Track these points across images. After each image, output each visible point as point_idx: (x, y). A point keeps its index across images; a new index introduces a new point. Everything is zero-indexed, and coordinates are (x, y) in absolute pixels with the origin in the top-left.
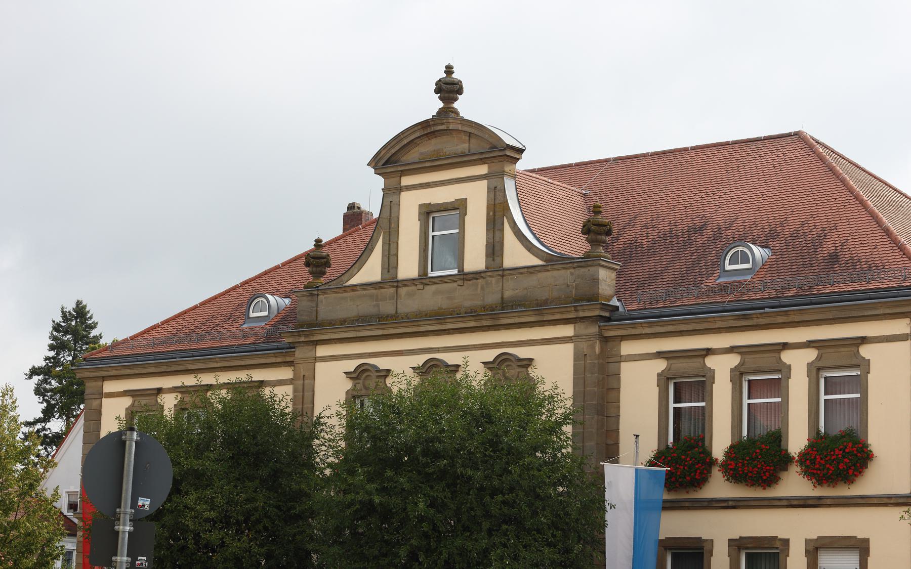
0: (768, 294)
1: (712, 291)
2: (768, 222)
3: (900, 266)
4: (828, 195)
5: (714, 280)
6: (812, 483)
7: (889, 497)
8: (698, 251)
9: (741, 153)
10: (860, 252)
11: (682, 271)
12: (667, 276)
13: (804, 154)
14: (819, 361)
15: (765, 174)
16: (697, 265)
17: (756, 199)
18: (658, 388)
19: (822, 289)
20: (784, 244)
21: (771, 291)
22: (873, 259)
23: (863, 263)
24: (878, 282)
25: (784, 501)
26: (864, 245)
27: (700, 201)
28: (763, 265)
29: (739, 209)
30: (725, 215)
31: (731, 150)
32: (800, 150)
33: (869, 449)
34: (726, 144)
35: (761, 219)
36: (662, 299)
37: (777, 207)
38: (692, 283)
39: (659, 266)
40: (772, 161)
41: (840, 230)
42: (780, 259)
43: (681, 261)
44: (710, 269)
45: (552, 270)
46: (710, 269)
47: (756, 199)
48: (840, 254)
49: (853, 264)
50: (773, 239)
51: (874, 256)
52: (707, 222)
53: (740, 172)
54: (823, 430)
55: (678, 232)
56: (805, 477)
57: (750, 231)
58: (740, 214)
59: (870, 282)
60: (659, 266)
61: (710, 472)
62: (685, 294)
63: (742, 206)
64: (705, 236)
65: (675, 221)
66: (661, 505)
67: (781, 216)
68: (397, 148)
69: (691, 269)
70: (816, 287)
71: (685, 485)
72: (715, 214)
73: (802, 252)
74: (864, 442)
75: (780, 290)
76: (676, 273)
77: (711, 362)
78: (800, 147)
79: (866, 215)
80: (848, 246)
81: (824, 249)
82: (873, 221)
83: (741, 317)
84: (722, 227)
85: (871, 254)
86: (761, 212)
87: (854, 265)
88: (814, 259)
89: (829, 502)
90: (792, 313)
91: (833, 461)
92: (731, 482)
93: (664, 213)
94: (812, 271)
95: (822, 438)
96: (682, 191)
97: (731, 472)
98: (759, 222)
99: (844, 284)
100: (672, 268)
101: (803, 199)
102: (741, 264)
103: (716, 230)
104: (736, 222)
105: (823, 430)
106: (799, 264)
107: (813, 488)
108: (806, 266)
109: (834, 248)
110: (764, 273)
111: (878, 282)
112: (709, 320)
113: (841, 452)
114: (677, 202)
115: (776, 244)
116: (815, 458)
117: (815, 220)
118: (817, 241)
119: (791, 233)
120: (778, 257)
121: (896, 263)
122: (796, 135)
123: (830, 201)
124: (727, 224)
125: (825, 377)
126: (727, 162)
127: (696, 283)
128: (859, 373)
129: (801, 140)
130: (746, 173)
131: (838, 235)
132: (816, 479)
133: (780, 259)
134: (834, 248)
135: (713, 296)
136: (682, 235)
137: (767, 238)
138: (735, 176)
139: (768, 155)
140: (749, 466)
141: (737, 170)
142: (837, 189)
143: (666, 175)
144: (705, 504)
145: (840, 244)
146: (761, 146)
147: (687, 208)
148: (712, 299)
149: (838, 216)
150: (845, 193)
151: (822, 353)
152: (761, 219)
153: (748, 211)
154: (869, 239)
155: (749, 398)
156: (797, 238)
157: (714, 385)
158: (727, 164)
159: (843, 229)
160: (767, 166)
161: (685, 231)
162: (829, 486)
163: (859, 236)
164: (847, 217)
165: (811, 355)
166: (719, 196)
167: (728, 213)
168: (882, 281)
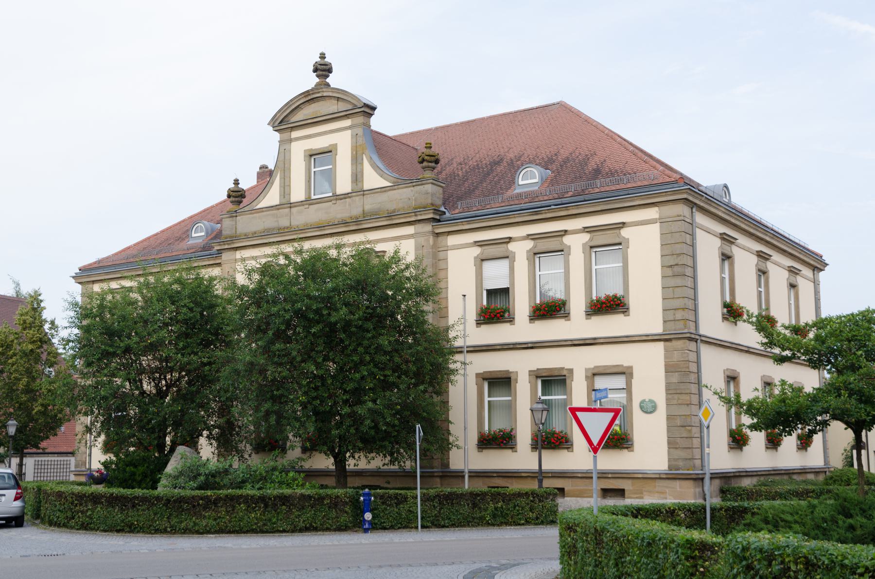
45: (398, 189)
68: (288, 111)
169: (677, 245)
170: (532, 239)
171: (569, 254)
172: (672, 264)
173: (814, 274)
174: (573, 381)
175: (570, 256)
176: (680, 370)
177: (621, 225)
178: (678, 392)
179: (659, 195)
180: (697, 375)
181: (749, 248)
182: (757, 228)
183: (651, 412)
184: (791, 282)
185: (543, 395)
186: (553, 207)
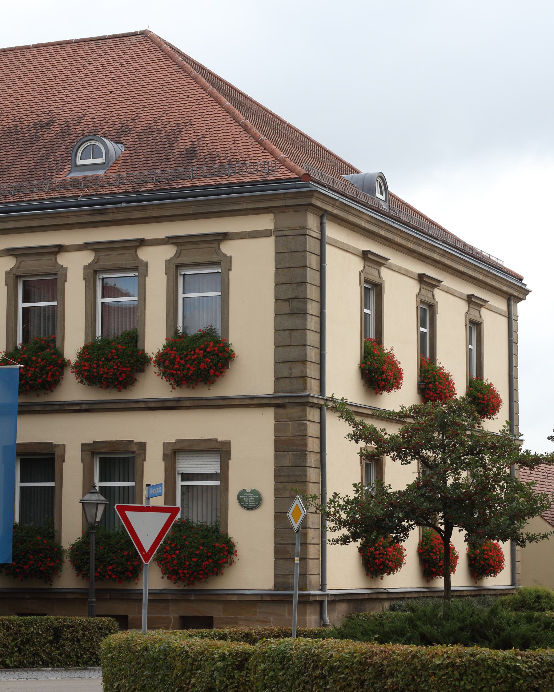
0: (124, 188)
1: (64, 185)
2: (118, 118)
3: (262, 161)
4: (180, 91)
5: (66, 175)
6: (171, 384)
7: (252, 398)
8: (46, 147)
9: (85, 51)
10: (218, 147)
11: (30, 166)
12: (15, 171)
13: (151, 53)
14: (178, 258)
15: (112, 71)
16: (46, 160)
17: (105, 96)
18: (6, 287)
19: (181, 184)
20: (138, 140)
21: (127, 186)
22: (232, 154)
23: (222, 158)
24: (240, 176)
25: (140, 403)
26: (222, 141)
27: (46, 98)
28: (116, 160)
29: (87, 105)
30: (72, 111)
31: (75, 48)
32: (147, 48)
33: (230, 348)
34: (70, 42)
35: (111, 115)
36: (152, 181)
37: (127, 103)
38: (42, 178)
39: (5, 161)
40: (119, 59)
41: (195, 126)
42: (134, 154)
43: (29, 157)
44: (59, 164)
46: (59, 164)
47: (105, 96)
48: (197, 149)
49: (211, 159)
50: (126, 134)
51: (233, 151)
52: (54, 118)
53: (86, 69)
54: (181, 330)
55: (24, 127)
56: (164, 378)
57: (100, 127)
58: (89, 110)
59: (232, 177)
60: (5, 161)
61: (61, 374)
62: (35, 189)
63: (90, 103)
64: (52, 132)
65: (19, 117)
66: (16, 409)
67: (132, 112)
69: (39, 164)
70: (175, 181)
71: (36, 387)
72: (62, 110)
73: (157, 147)
74: (225, 342)
75: (137, 185)
76: (23, 168)
77: (63, 260)
78: (147, 46)
79: (221, 112)
80: (205, 142)
81: (180, 145)
82: (229, 116)
83: (95, 212)
84: (70, 123)
85: (230, 150)
86: (111, 108)
87: (213, 160)
88: (170, 154)
89: (188, 404)
90: (151, 207)
91: (194, 360)
92: (85, 384)
93: (7, 109)
94: (169, 166)
95: (181, 338)
96: (25, 88)
97: (86, 374)
98: (109, 118)
99: (204, 179)
100: (19, 163)
101: (154, 96)
102: (93, 158)
103: (63, 126)
104: (85, 118)
105: (181, 330)
106: (154, 159)
107: (171, 389)
108: (162, 161)
109: (190, 143)
110: (118, 167)
111: (240, 176)
112: (62, 215)
113: (203, 351)
114: (21, 98)
115: (129, 139)
116: (174, 358)
117: (168, 116)
118: (172, 136)
119: (144, 128)
120: (132, 152)
121: (257, 158)
122: (143, 34)
123: (182, 97)
124: (75, 119)
125: (183, 275)
126: (71, 60)
127: (46, 178)
128: (220, 271)
129: (148, 39)
130: (92, 70)
131: (193, 131)
132: (175, 380)
133: (134, 154)
134: (190, 143)
135: (65, 191)
136: (28, 130)
137: (119, 134)
138: (81, 73)
139: (114, 53)
140: (105, 367)
141: (82, 68)
142: (189, 86)
143: (8, 72)
144: (57, 407)
145: (196, 139)
146: (106, 45)
147: (32, 104)
148: (65, 193)
149: (192, 112)
150: (198, 90)
151: (181, 250)
152: (111, 115)
153: (97, 107)
154: (227, 134)
155: (103, 297)
156: (150, 133)
157: (66, 283)
158: (71, 61)
159: (199, 125)
160: (114, 64)
161: (30, 127)
162: (188, 387)
163: (216, 132)
164: (202, 113)
165: (169, 252)
166: (65, 93)
167: (75, 109)
168: (244, 175)
169: (298, 269)
170: (92, 250)
171: (146, 275)
172: (290, 297)
173: (509, 306)
174: (145, 460)
175: (147, 278)
176: (295, 448)
177: (221, 237)
178: (292, 479)
179: (237, 201)
180: (319, 455)
181: (407, 270)
182: (419, 242)
183: (253, 508)
184: (472, 317)
185: (101, 480)
186: (124, 204)
